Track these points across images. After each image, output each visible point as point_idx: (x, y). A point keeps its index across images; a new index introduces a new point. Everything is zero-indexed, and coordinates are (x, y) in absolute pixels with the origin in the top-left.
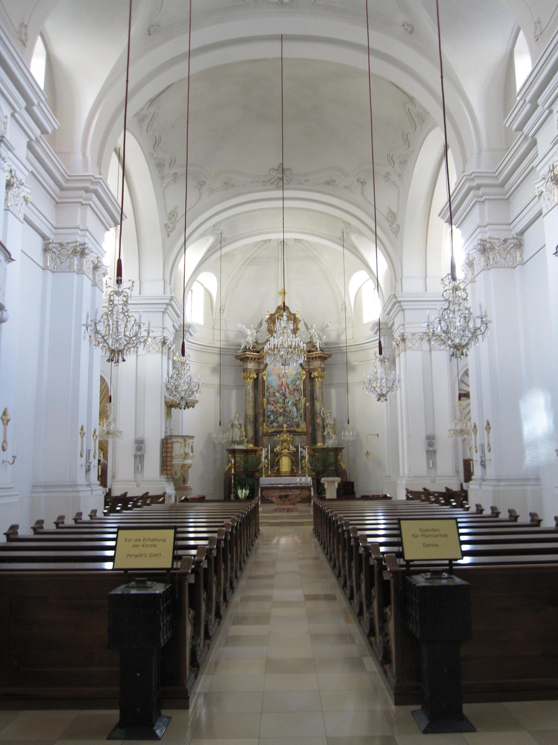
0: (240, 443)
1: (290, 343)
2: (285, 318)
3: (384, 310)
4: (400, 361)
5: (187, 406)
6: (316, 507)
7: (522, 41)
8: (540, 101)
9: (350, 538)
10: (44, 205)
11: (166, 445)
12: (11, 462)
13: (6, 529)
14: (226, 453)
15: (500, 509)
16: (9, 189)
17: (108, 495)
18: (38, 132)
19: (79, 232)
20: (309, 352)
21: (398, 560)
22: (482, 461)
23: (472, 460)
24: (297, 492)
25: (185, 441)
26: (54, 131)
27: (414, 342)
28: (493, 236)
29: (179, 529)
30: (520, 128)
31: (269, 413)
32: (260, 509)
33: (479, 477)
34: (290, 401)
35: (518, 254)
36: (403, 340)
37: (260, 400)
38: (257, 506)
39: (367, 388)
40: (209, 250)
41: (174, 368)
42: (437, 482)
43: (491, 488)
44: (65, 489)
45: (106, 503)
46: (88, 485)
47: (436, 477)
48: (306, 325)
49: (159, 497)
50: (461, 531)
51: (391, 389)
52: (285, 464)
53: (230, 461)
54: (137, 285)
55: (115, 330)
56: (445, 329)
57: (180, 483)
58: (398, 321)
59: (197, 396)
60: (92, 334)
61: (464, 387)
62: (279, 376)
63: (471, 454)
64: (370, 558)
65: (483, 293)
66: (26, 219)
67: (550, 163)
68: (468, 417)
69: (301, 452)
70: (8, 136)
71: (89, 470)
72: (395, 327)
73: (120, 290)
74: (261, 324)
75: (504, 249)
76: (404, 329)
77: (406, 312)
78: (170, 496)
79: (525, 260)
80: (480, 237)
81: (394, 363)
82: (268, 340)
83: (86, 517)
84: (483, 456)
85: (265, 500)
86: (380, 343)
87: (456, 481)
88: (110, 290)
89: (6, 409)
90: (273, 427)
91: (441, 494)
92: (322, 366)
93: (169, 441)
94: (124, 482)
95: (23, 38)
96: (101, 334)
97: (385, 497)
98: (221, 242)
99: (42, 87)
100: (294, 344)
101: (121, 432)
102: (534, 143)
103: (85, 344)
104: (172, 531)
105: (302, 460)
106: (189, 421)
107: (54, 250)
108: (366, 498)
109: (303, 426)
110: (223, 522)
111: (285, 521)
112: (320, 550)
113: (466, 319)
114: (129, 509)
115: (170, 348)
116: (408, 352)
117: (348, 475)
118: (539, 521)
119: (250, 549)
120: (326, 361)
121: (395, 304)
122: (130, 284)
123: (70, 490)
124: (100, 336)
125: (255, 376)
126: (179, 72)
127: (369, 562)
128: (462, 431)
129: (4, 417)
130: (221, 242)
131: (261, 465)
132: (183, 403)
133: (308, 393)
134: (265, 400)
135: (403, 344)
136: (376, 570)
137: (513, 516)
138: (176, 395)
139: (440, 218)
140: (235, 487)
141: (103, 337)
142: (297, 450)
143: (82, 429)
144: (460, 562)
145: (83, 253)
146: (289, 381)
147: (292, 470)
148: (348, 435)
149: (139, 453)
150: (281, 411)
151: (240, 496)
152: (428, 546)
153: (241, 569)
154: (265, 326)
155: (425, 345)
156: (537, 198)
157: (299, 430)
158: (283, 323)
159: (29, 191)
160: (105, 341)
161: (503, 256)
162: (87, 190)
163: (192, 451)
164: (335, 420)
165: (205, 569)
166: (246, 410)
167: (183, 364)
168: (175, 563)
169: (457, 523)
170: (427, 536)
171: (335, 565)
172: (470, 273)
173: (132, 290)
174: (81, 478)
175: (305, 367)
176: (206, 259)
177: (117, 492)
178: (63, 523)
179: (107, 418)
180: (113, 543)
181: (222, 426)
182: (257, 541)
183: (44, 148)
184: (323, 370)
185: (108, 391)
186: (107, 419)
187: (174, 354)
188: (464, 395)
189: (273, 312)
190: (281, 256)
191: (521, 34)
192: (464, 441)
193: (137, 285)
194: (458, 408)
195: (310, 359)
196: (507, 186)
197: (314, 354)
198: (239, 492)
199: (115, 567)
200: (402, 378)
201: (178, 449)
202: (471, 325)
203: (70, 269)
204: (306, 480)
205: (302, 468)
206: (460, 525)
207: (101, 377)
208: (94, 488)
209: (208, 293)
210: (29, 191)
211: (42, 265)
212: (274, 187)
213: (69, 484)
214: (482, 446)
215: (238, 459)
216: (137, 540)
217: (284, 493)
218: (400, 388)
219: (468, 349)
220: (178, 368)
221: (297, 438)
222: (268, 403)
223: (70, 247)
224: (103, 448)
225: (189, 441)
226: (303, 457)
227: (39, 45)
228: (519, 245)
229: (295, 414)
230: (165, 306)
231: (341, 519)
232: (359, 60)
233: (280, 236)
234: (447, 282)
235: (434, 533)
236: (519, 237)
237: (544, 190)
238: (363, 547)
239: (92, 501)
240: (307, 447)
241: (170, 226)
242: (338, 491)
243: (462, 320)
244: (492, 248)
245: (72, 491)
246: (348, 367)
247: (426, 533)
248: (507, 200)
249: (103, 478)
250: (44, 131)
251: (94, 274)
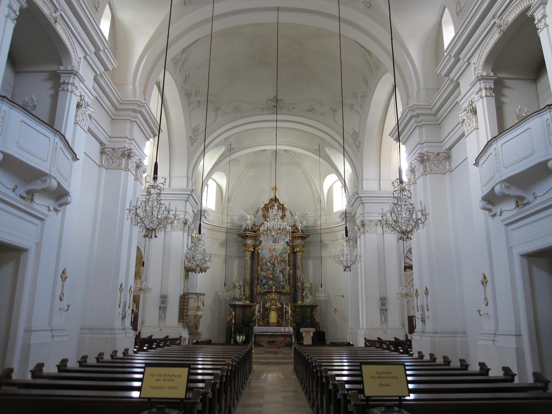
0: (239, 300)
1: (279, 226)
2: (276, 208)
3: (348, 202)
4: (361, 241)
5: (201, 271)
6: (296, 351)
7: (447, 15)
8: (461, 56)
9: (322, 376)
10: (104, 121)
11: (184, 299)
12: (66, 310)
13: (58, 363)
14: (229, 307)
15: (437, 356)
16: (79, 109)
17: (138, 337)
18: (102, 69)
19: (128, 141)
20: (293, 233)
21: (359, 395)
22: (422, 318)
23: (415, 317)
24: (282, 339)
25: (198, 297)
26: (114, 68)
27: (371, 227)
28: (429, 151)
29: (192, 366)
30: (447, 75)
31: (262, 278)
32: (253, 351)
33: (421, 330)
34: (278, 269)
35: (447, 164)
36: (363, 225)
37: (255, 268)
38: (251, 349)
39: (336, 261)
40: (221, 156)
41: (192, 242)
42: (388, 333)
43: (430, 339)
44: (104, 332)
45: (136, 344)
46: (123, 329)
47: (387, 329)
48: (291, 213)
49: (176, 339)
50: (408, 372)
51: (354, 262)
52: (273, 317)
53: (231, 314)
54: (167, 181)
55: (150, 214)
56: (395, 219)
57: (193, 330)
58: (359, 212)
59: (209, 264)
60: (133, 216)
61: (408, 261)
62: (270, 251)
63: (414, 312)
64: (338, 393)
65: (422, 194)
66: (89, 130)
67: (470, 99)
68: (411, 284)
69: (286, 308)
70: (80, 72)
71: (125, 317)
72: (357, 215)
73: (156, 185)
74: (258, 211)
75: (437, 160)
76: (364, 217)
77: (365, 204)
78: (185, 339)
79: (453, 168)
80: (419, 151)
81: (356, 242)
82: (263, 223)
83: (120, 354)
84: (423, 314)
85: (257, 345)
86: (346, 227)
87: (402, 333)
88: (148, 184)
89: (65, 269)
90: (265, 289)
91: (391, 343)
92: (303, 243)
93: (186, 297)
94: (151, 327)
95: (96, 5)
96: (140, 217)
97: (349, 344)
98: (230, 151)
99: (107, 37)
100: (282, 227)
101: (150, 289)
102: (458, 85)
103: (127, 224)
104: (187, 369)
105: (286, 314)
106: (201, 282)
107: (108, 153)
108: (334, 344)
109: (287, 288)
110: (225, 361)
111: (272, 361)
112: (298, 384)
113: (411, 212)
114: (154, 349)
115: (190, 227)
116: (367, 234)
117: (320, 326)
118: (467, 366)
119: (244, 383)
120: (305, 240)
121: (356, 198)
122: (163, 181)
123: (109, 332)
124: (139, 218)
125: (253, 250)
126: (205, 30)
127: (347, 408)
128: (407, 295)
129: (63, 275)
130: (230, 151)
131: (255, 317)
132: (198, 269)
133: (291, 263)
134: (259, 268)
135: (363, 228)
136: (342, 403)
137: (447, 362)
138: (192, 263)
139: (390, 137)
140: (235, 334)
141: (141, 219)
142: (283, 307)
143: (121, 286)
144: (407, 398)
145: (129, 156)
146: (277, 254)
147: (279, 321)
148: (321, 296)
149: (163, 305)
150: (271, 276)
151: (238, 340)
152: (383, 385)
153: (237, 398)
154: (261, 212)
155: (379, 229)
156: (460, 124)
157: (285, 291)
158: (274, 211)
159: (93, 110)
160: (143, 222)
161: (437, 165)
162: (135, 111)
163: (203, 306)
164: (311, 284)
165: (210, 399)
166: (245, 275)
167: (199, 240)
168: (188, 394)
169: (405, 366)
170: (382, 378)
171: (310, 397)
172: (412, 177)
173: (164, 185)
174: (118, 323)
175: (290, 244)
176: (219, 163)
177: (145, 335)
178: (102, 358)
179: (140, 278)
180: (140, 376)
181: (227, 287)
182: (250, 376)
183: (106, 81)
184: (303, 246)
185: (142, 258)
186: (140, 279)
187: (193, 232)
188: (408, 267)
189: (267, 202)
190: (274, 162)
191: (446, 10)
192: (408, 302)
193: (167, 181)
194: (403, 277)
195: (294, 238)
196: (439, 115)
197: (296, 235)
198: (238, 337)
199: (142, 396)
200: (362, 254)
201: (192, 303)
202: (414, 217)
203: (119, 168)
204: (289, 329)
205: (286, 320)
206: (407, 368)
207: (138, 247)
208: (128, 332)
209: (219, 187)
210: (93, 110)
211: (98, 163)
212: (270, 112)
213: (109, 328)
214: (422, 306)
215: (237, 312)
216: (159, 375)
217: (272, 340)
218: (361, 261)
219: (412, 234)
220: (195, 242)
221: (282, 297)
222: (262, 270)
223: (120, 152)
224: (136, 300)
225: (201, 297)
226: (287, 312)
227: (107, 11)
228: (448, 157)
229: (282, 279)
230: (187, 196)
231: (315, 361)
232: (332, 26)
233: (274, 147)
234: (396, 185)
235: (387, 375)
236: (449, 152)
237: (466, 118)
238: (332, 384)
239: (125, 341)
240: (290, 304)
241: (194, 138)
242: (313, 338)
243: (408, 212)
244: (428, 160)
245: (110, 334)
246: (322, 244)
247: (381, 375)
248: (439, 125)
249: (134, 324)
250: (106, 69)
251: (136, 171)
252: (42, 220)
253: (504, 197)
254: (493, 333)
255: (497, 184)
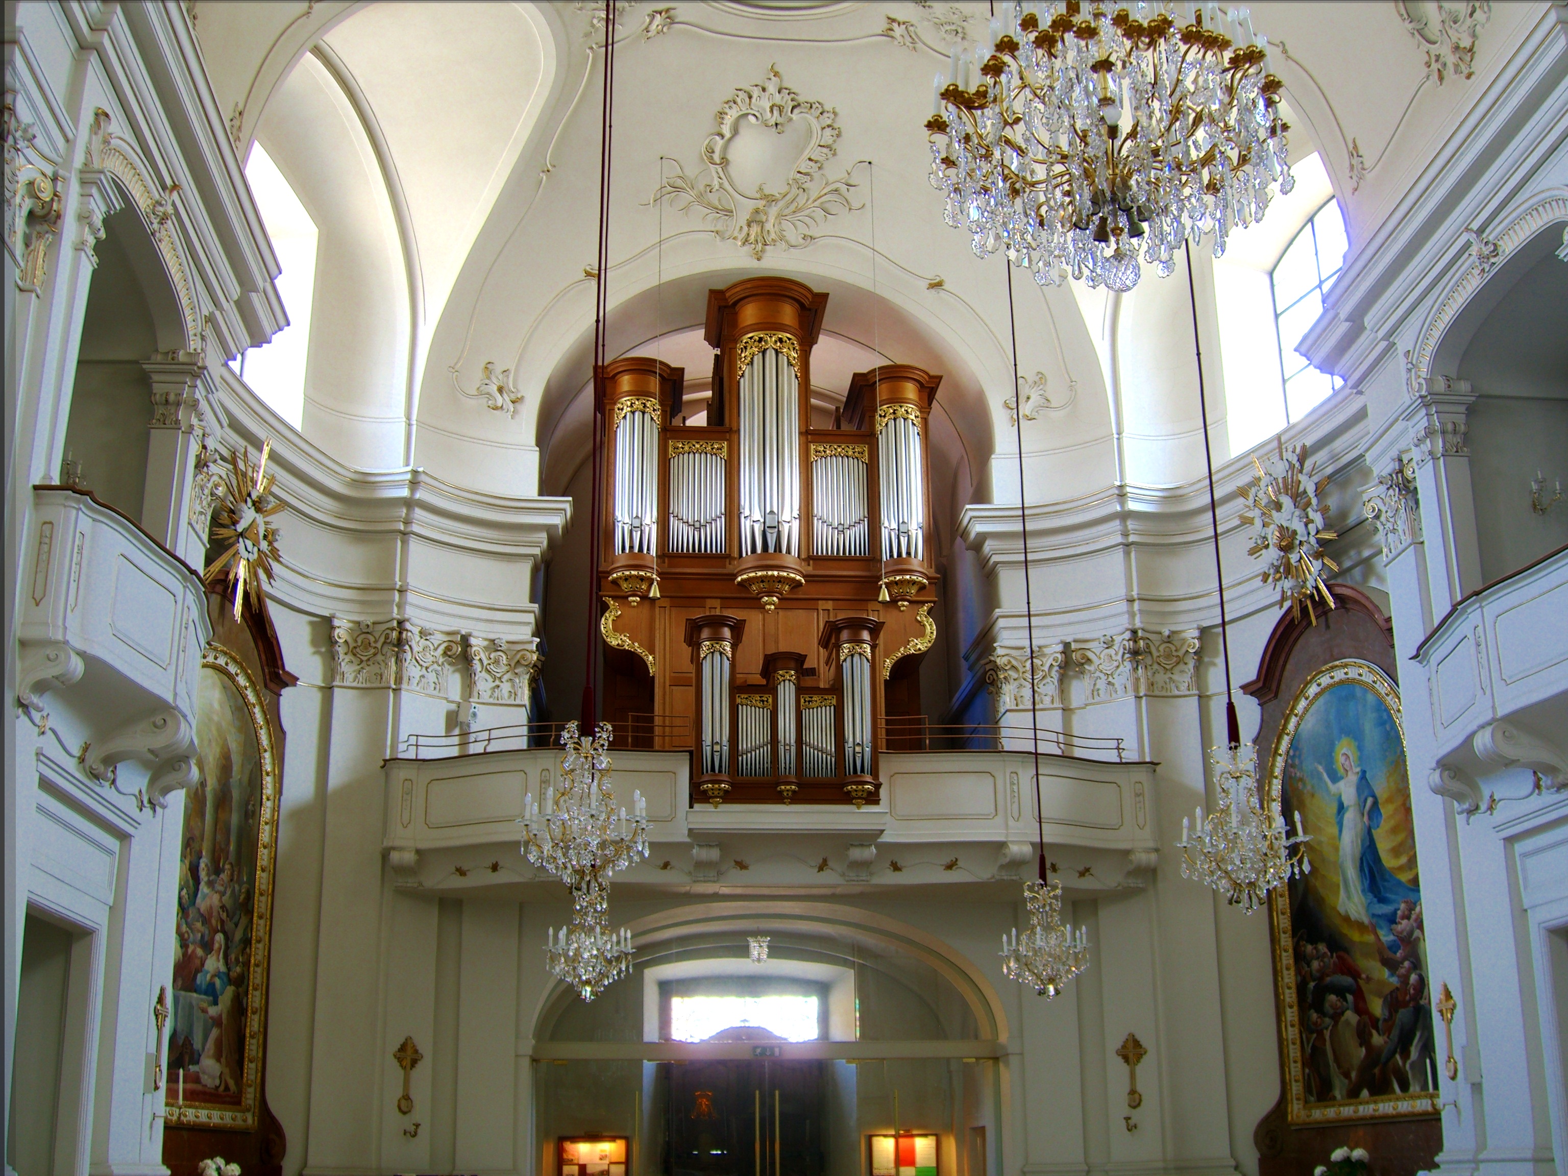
252: (123, 837)
253: (1500, 764)
254: (1471, 1157)
255: (1482, 727)
